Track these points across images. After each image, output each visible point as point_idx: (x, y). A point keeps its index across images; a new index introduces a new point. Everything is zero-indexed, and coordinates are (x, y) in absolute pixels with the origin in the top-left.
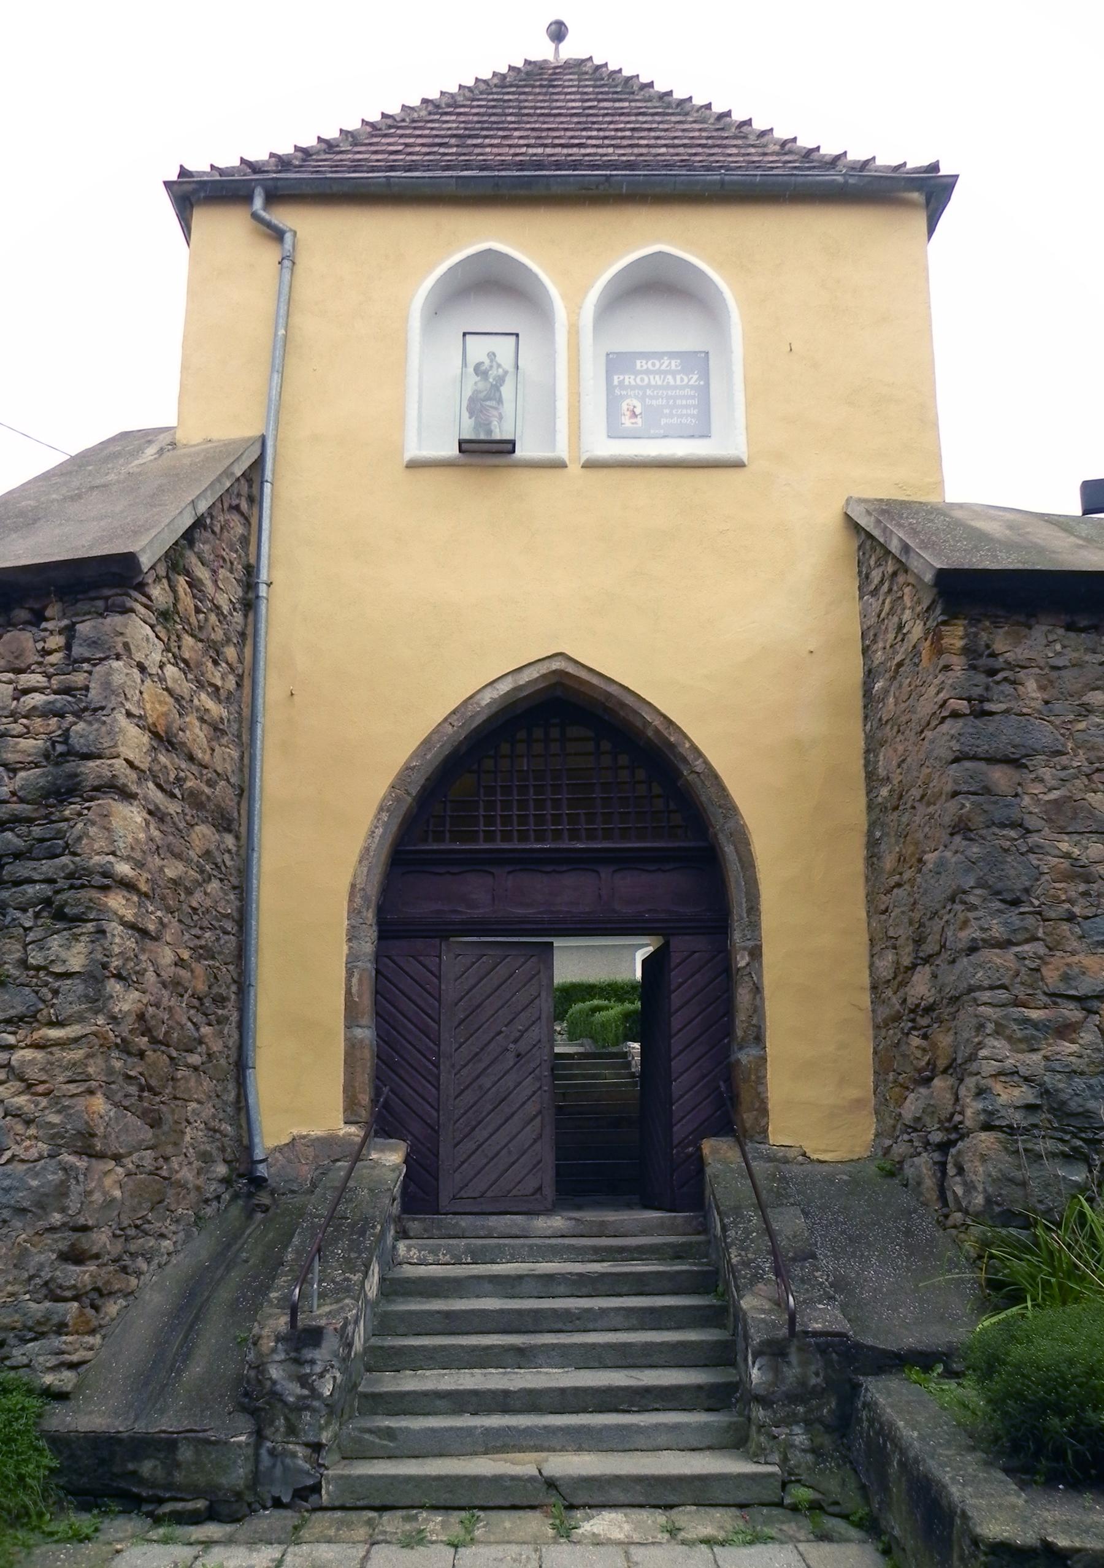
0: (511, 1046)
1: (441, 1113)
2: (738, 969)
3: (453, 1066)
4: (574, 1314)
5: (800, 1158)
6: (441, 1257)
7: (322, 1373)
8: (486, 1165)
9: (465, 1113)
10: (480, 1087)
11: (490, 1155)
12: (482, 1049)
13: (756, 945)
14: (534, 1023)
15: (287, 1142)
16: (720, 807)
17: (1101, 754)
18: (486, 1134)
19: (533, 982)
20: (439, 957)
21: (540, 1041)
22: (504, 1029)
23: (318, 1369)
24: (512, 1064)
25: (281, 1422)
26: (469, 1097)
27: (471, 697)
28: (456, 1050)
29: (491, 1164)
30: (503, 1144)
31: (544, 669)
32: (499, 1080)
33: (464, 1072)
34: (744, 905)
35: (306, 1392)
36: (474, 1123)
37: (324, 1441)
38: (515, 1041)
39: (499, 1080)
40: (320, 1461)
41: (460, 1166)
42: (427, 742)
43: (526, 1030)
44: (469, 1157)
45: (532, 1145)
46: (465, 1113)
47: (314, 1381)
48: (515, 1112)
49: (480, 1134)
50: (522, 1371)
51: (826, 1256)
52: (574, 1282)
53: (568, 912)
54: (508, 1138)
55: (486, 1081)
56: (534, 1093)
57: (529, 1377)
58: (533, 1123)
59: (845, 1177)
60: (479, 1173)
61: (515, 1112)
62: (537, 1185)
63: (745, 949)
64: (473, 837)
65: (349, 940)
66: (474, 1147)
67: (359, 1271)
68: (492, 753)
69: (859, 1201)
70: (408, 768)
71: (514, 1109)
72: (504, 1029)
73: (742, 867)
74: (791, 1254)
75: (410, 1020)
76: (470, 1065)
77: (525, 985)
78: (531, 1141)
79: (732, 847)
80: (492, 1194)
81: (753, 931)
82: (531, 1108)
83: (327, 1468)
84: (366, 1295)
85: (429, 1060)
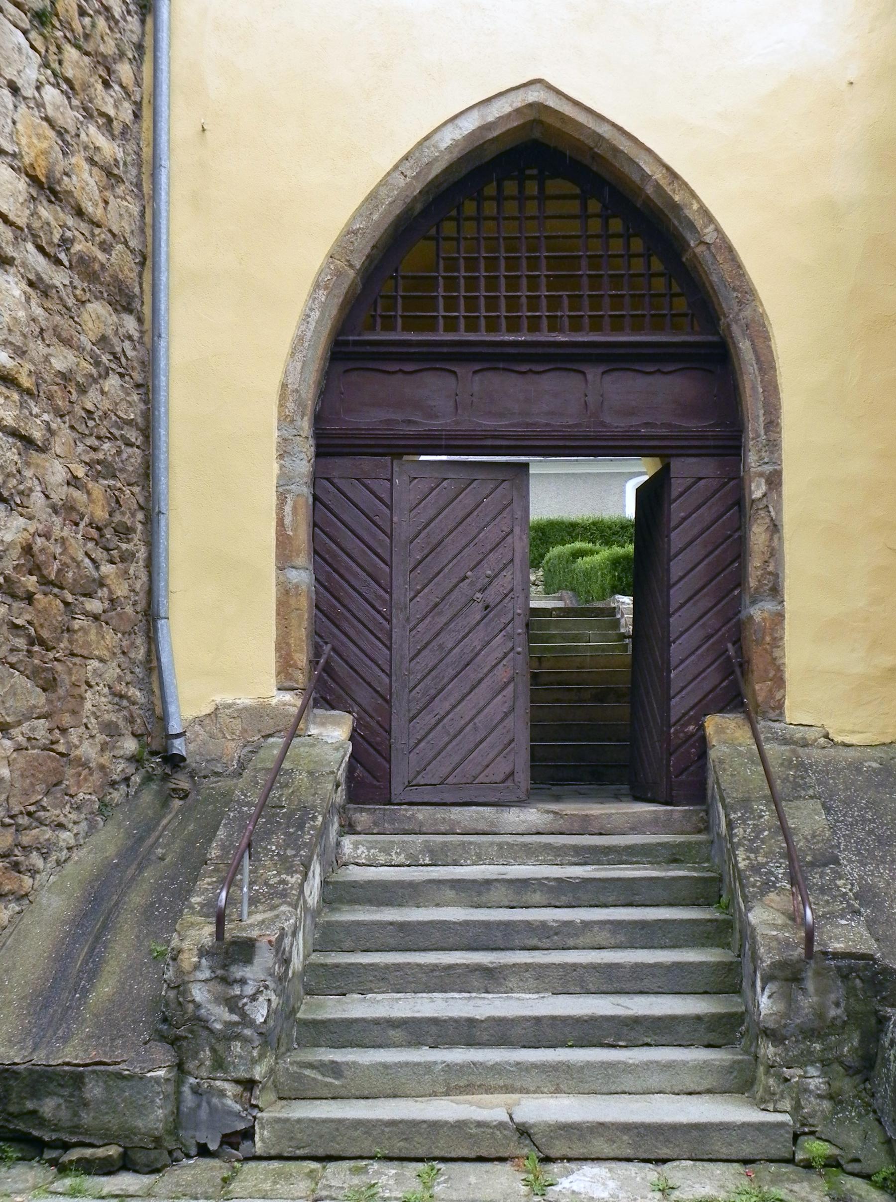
0: (478, 595)
1: (394, 678)
2: (753, 501)
3: (408, 620)
6: (394, 857)
7: (254, 995)
8: (447, 744)
10: (441, 646)
11: (452, 732)
12: (443, 599)
13: (775, 470)
14: (505, 566)
15: (208, 712)
16: (734, 289)
18: (447, 706)
19: (504, 514)
20: (391, 480)
21: (512, 590)
24: (478, 617)
27: (427, 138)
28: (411, 600)
29: (454, 743)
30: (467, 719)
32: (464, 638)
33: (421, 627)
34: (762, 419)
35: (235, 1018)
36: (433, 692)
37: (257, 1078)
38: (483, 590)
39: (464, 638)
40: (254, 1102)
41: (417, 744)
42: (373, 197)
43: (496, 576)
45: (502, 720)
48: (482, 679)
49: (441, 706)
51: (850, 861)
53: (547, 425)
54: (474, 711)
55: (447, 640)
58: (504, 693)
59: (875, 765)
60: (439, 753)
61: (482, 679)
62: (508, 770)
63: (761, 475)
64: (430, 324)
65: (281, 457)
66: (433, 721)
68: (454, 213)
70: (350, 232)
71: (480, 675)
72: (469, 573)
73: (760, 369)
74: (809, 858)
76: (429, 619)
77: (494, 519)
79: (748, 343)
80: (455, 781)
81: (772, 452)
82: (502, 674)
84: (305, 902)
85: (379, 612)
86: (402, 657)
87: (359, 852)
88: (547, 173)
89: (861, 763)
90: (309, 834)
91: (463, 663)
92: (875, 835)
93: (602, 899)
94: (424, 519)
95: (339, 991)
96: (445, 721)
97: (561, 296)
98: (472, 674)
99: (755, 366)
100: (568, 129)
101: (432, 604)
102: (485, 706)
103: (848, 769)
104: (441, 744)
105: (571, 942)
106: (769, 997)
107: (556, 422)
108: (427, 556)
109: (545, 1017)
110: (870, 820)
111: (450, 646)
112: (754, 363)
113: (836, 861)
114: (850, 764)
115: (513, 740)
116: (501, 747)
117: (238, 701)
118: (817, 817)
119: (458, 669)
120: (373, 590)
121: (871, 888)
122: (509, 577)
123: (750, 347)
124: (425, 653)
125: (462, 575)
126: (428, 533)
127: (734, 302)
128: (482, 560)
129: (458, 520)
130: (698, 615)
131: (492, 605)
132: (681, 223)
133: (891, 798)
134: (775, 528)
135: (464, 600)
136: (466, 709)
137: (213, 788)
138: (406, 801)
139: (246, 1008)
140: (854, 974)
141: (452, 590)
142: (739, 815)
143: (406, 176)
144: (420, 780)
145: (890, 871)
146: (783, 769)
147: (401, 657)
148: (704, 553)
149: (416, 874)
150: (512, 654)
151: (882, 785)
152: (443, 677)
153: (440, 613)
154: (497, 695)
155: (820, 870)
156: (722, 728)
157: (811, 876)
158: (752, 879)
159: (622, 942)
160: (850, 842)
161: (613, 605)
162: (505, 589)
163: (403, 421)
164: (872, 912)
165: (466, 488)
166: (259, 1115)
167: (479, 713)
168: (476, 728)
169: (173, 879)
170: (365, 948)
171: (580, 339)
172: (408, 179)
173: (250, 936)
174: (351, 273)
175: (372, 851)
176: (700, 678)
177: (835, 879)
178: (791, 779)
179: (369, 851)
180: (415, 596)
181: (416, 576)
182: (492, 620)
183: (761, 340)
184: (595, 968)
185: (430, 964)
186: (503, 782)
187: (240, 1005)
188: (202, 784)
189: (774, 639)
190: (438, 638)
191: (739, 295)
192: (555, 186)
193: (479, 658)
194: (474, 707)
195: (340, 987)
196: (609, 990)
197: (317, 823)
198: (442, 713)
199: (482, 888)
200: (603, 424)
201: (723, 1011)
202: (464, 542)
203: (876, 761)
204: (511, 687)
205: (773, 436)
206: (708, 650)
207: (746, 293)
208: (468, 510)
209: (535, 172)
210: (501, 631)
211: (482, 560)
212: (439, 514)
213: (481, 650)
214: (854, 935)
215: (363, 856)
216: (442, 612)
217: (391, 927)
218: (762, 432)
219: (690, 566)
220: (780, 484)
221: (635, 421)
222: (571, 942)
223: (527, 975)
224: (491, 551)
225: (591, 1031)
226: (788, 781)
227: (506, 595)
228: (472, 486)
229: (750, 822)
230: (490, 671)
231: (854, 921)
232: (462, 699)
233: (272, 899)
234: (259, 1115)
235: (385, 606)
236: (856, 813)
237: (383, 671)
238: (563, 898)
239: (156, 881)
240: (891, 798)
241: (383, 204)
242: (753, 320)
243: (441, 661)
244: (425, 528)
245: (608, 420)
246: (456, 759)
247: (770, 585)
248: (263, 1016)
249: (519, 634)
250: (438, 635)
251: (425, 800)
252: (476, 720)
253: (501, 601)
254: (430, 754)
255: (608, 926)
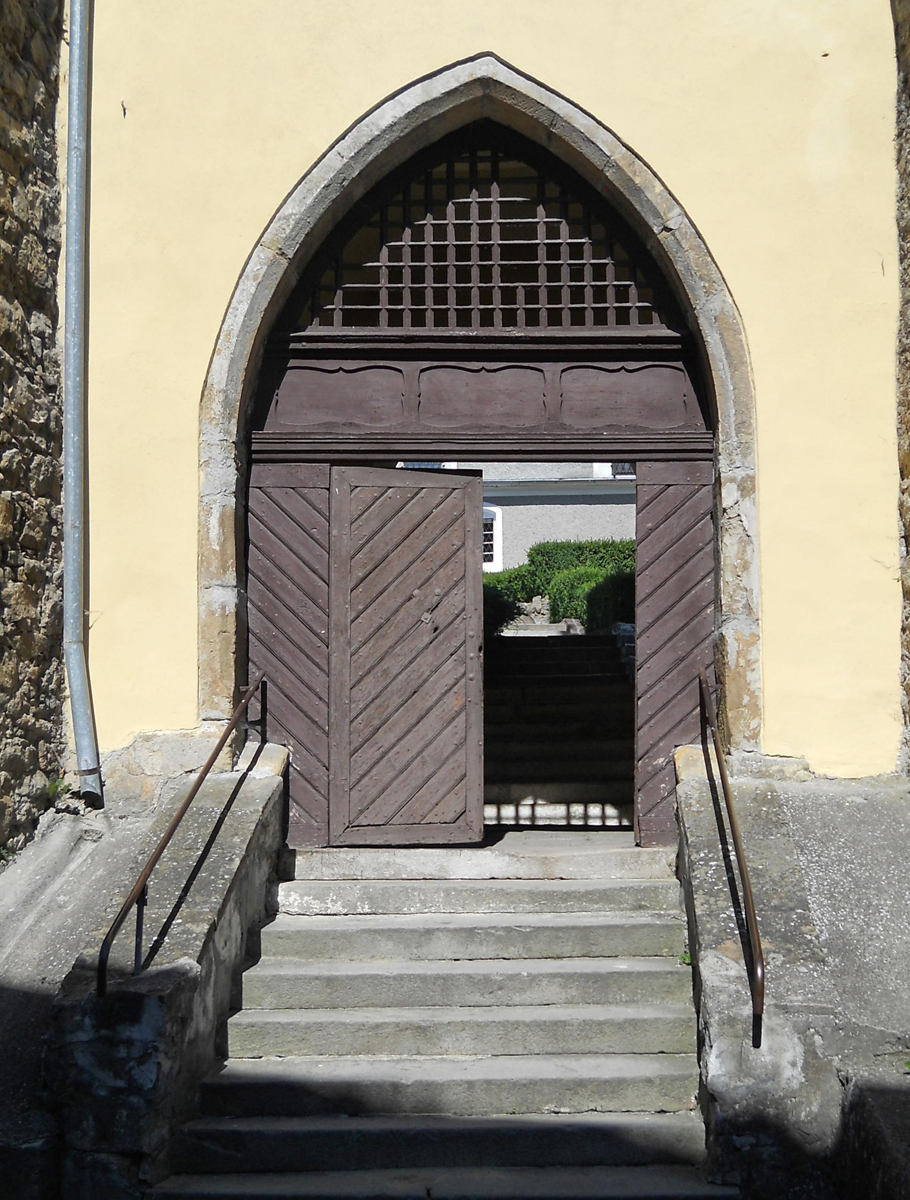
0: (426, 615)
1: (333, 707)
2: (725, 510)
3: (349, 643)
4: (495, 982)
5: (802, 773)
6: (330, 905)
7: (141, 1057)
8: (394, 779)
9: (365, 709)
10: (385, 672)
11: (398, 766)
12: (388, 620)
13: (748, 476)
14: (456, 584)
15: (125, 745)
16: (701, 278)
17: (908, 123)
18: (392, 738)
19: (455, 527)
21: (464, 610)
22: (416, 592)
23: (136, 1052)
24: (427, 640)
25: (89, 1124)
26: (370, 686)
28: (352, 621)
29: (400, 779)
30: (414, 752)
31: (463, 75)
32: (411, 662)
33: (364, 651)
34: (733, 419)
35: (120, 1083)
36: (376, 722)
37: (146, 1149)
38: (432, 610)
39: (411, 662)
40: (141, 1176)
41: (360, 780)
43: (446, 594)
44: (371, 768)
45: (453, 753)
46: (365, 709)
47: (132, 1068)
48: (431, 708)
49: (386, 738)
50: (423, 1057)
51: (821, 905)
52: (499, 939)
53: (502, 427)
54: (422, 744)
55: (393, 664)
56: (457, 681)
57: (428, 1066)
58: (454, 724)
59: (859, 800)
60: (383, 791)
61: (431, 708)
62: (459, 809)
63: (732, 480)
64: (371, 319)
66: (377, 755)
67: (203, 921)
68: (400, 197)
69: (873, 831)
71: (429, 704)
72: (416, 592)
73: (730, 365)
74: (775, 902)
75: (290, 578)
76: (372, 642)
77: (444, 531)
78: (453, 747)
79: (717, 337)
80: (401, 821)
81: (745, 456)
82: (453, 702)
83: (150, 1185)
84: (217, 954)
85: (316, 634)
86: (342, 685)
87: (291, 899)
88: (500, 155)
89: (843, 798)
90: (223, 878)
91: (410, 690)
92: (852, 877)
93: (557, 951)
94: (367, 532)
95: (255, 1054)
96: (390, 754)
97: (517, 287)
98: (420, 703)
99: (725, 360)
100: (521, 107)
101: (375, 625)
102: (435, 738)
103: (828, 804)
104: (386, 780)
105: (517, 999)
106: (718, 1057)
107: (512, 424)
108: (370, 573)
109: (479, 1080)
110: (847, 860)
111: (395, 672)
112: (724, 358)
113: (805, 905)
114: (833, 798)
115: (465, 775)
116: (452, 783)
117: (159, 733)
118: (787, 857)
119: (404, 698)
120: (310, 612)
121: (842, 935)
122: (460, 596)
123: (719, 341)
124: (369, 679)
125: (408, 594)
126: (371, 547)
127: (701, 293)
128: (430, 577)
129: (405, 533)
130: (667, 637)
131: (442, 627)
132: (642, 206)
133: (873, 835)
134: (747, 539)
135: (411, 621)
136: (413, 742)
137: (129, 830)
138: (347, 843)
139: (133, 1072)
140: (812, 1030)
141: (397, 610)
142: (702, 855)
143: (343, 157)
144: (363, 820)
145: (865, 916)
146: (756, 805)
147: (341, 684)
148: (672, 567)
149: (351, 923)
150: (464, 680)
151: (864, 822)
152: (388, 706)
153: (384, 636)
154: (447, 726)
155: (785, 915)
156: (693, 760)
157: (775, 921)
158: (708, 926)
159: (573, 997)
160: (822, 884)
161: (614, 633)
162: (456, 608)
163: (344, 425)
164: (841, 962)
165: (412, 498)
166: (148, 1191)
167: (427, 746)
168: (424, 763)
169: (72, 929)
170: (288, 1005)
171: (537, 334)
172: (345, 160)
173: (138, 991)
174: (285, 263)
175: (306, 898)
176: (670, 705)
177: (801, 925)
178: (764, 815)
179: (302, 899)
180: (358, 617)
181: (358, 595)
182: (442, 643)
183: (731, 333)
184: (539, 1026)
185: (356, 1023)
186: (454, 823)
187: (127, 1069)
188: (118, 825)
189: (748, 662)
190: (383, 663)
191: (707, 285)
192: (508, 166)
193: (427, 684)
194: (422, 739)
195: (252, 1050)
196: (554, 1051)
197: (233, 866)
198: (387, 745)
199: (423, 938)
200: (563, 426)
201: (676, 1073)
202: (411, 557)
203: (860, 795)
204: (462, 716)
205: (744, 438)
206: (679, 674)
207: (714, 282)
208: (415, 522)
209: (488, 153)
210: (452, 655)
211: (430, 577)
212: (383, 527)
213: (430, 676)
214: (815, 986)
215: (296, 904)
216: (387, 634)
217: (317, 981)
218: (733, 434)
219: (658, 583)
220: (753, 489)
221: (597, 423)
222: (517, 999)
223: (464, 1034)
224: (441, 567)
225: (530, 1097)
226: (760, 818)
227: (458, 616)
228: (419, 495)
229: (713, 863)
230: (439, 699)
231: (817, 971)
232: (409, 731)
233: (173, 950)
234: (148, 1191)
235: (322, 628)
236: (833, 853)
237: (321, 699)
238: (512, 949)
239: (53, 933)
240: (873, 835)
241: (318, 187)
242: (722, 312)
243: (386, 688)
244: (367, 542)
245: (568, 421)
246: (403, 796)
247: (744, 601)
248: (151, 1081)
249: (471, 659)
250: (382, 659)
251: (368, 843)
252: (424, 754)
253: (452, 622)
254: (374, 792)
255: (557, 979)
